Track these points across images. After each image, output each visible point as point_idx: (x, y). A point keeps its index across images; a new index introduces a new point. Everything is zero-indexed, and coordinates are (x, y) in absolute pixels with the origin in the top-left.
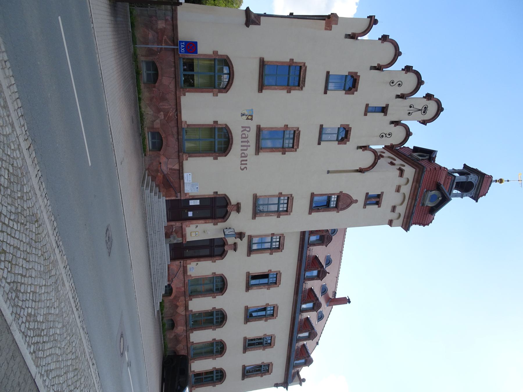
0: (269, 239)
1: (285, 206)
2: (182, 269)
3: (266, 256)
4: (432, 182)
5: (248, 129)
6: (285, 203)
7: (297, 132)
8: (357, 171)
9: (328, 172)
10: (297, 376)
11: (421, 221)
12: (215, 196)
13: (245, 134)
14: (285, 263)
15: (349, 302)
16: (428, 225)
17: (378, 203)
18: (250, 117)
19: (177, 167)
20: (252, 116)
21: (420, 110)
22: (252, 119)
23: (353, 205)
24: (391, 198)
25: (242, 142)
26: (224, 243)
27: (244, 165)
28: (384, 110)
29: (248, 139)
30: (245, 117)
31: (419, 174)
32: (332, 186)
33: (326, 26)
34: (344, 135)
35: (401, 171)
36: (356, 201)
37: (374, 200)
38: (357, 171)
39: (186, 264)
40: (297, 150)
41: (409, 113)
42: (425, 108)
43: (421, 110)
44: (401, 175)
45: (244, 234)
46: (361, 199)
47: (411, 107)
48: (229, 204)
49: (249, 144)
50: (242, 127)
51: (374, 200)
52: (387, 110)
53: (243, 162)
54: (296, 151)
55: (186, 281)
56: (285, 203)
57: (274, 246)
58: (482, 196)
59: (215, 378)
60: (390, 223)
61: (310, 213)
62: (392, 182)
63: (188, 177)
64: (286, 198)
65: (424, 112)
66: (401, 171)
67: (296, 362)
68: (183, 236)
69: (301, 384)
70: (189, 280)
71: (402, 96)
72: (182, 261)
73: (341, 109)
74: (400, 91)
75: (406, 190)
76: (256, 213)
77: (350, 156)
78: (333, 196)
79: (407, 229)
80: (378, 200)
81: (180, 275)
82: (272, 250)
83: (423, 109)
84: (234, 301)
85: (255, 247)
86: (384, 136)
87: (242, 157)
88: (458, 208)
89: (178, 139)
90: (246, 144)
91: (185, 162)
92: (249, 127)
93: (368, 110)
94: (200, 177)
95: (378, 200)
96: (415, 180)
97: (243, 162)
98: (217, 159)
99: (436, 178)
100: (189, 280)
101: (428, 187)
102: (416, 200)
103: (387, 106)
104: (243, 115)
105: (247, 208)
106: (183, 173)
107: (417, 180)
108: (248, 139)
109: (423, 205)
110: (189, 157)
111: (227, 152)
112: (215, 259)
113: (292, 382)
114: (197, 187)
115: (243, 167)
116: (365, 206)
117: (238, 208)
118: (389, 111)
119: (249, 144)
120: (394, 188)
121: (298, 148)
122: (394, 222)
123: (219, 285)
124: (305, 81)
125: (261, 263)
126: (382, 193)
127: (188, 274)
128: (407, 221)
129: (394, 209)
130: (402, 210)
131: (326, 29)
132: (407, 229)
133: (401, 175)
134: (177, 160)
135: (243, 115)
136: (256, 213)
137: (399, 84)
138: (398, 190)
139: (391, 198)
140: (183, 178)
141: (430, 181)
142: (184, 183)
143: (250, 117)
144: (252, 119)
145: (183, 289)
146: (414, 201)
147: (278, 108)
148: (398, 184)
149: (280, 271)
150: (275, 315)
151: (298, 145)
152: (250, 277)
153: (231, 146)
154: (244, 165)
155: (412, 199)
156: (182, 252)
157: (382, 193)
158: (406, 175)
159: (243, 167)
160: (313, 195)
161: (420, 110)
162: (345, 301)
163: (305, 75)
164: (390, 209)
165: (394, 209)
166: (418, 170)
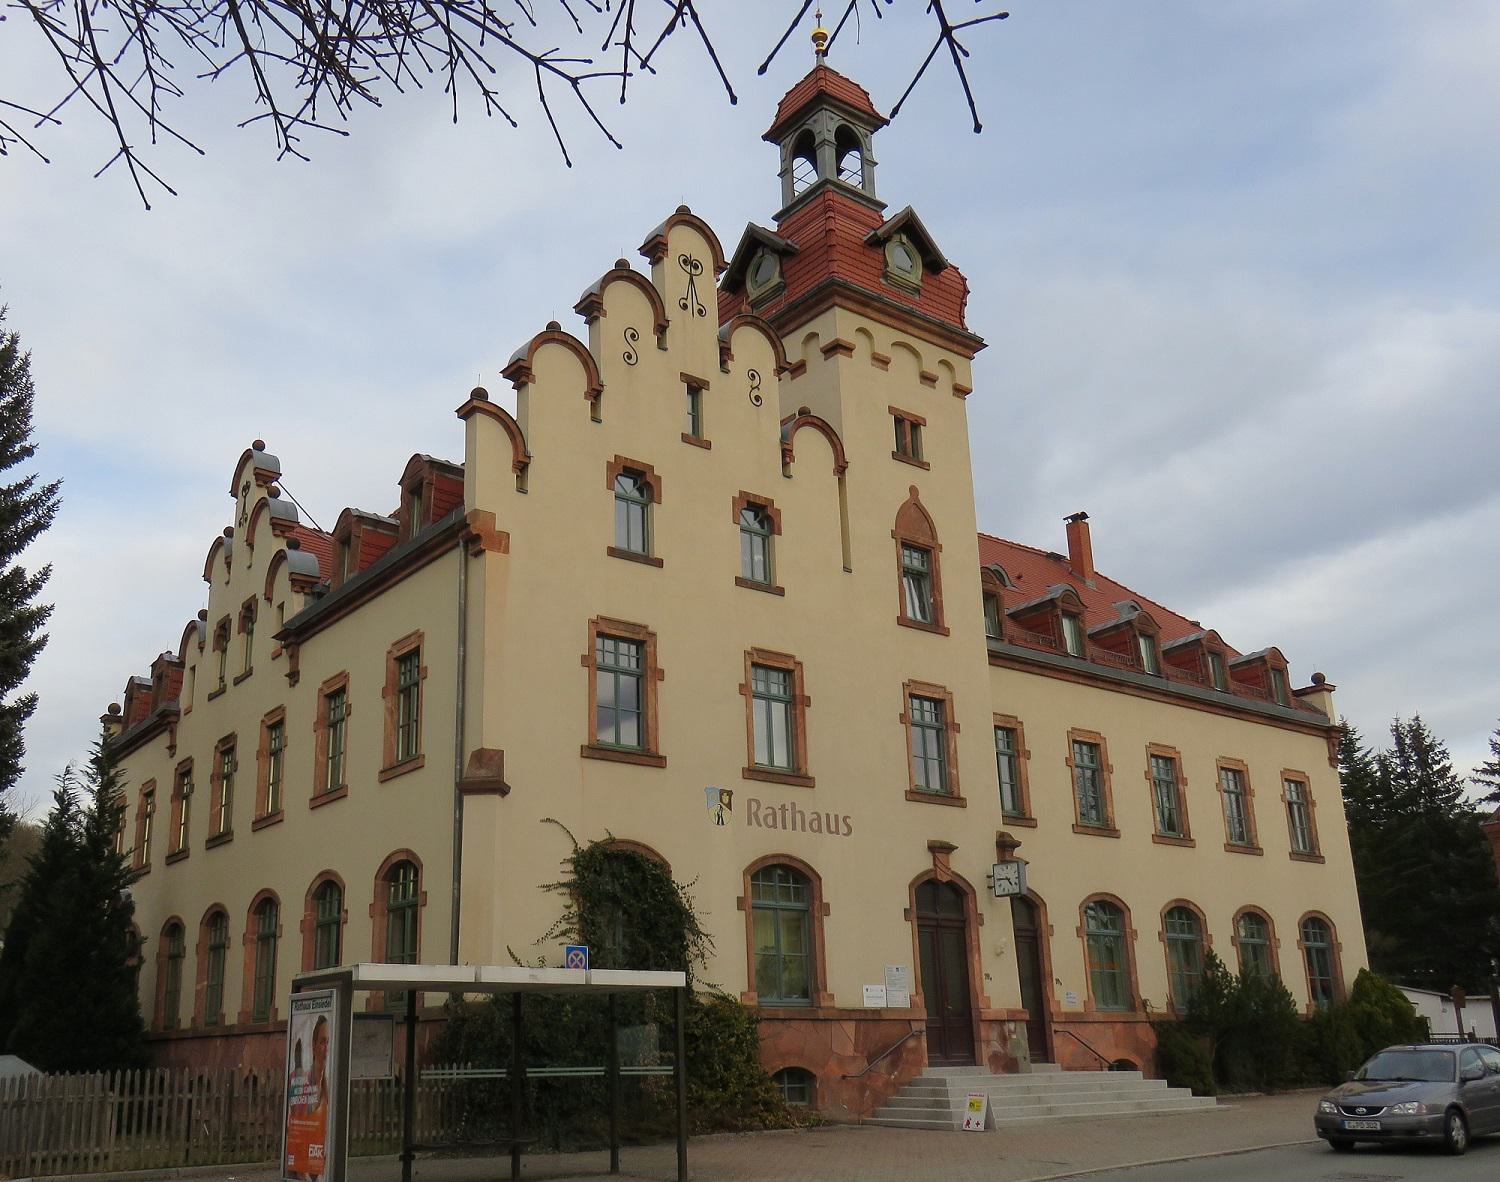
0: (606, 681)
1: (931, 711)
2: (1071, 1028)
3: (668, 699)
4: (863, 258)
5: (754, 804)
6: (616, 648)
7: (756, 659)
8: (841, 482)
9: (847, 569)
10: (1305, 699)
11: (954, 299)
12: (914, 916)
13: (766, 817)
14: (1055, 710)
15: (1084, 516)
16: (964, 280)
17: (916, 425)
18: (726, 799)
19: (850, 1028)
20: (722, 792)
21: (691, 280)
22: (730, 793)
23: (924, 500)
24: (901, 387)
25: (784, 827)
26: (929, 882)
27: (835, 825)
28: (695, 387)
29: (777, 807)
30: (726, 813)
31: (848, 298)
32: (881, 560)
33: (499, 550)
34: (761, 515)
35: (835, 348)
36: (913, 490)
37: (908, 431)
38: (841, 482)
39: (1060, 1014)
40: (798, 659)
41: (700, 312)
42: (685, 262)
43: (691, 276)
44: (848, 349)
45: (1001, 835)
46: (907, 474)
47: (685, 307)
48: (932, 875)
49: (788, 806)
50: (750, 823)
51: (908, 431)
52: (696, 380)
53: (833, 829)
54: (800, 664)
55: (1099, 1016)
56: (616, 648)
57: (1232, 784)
58: (871, 104)
59: (1320, 944)
60: (961, 391)
61: (945, 633)
62: (867, 374)
63: (874, 997)
64: (599, 641)
65: (696, 267)
66: (835, 348)
67: (1146, 668)
68: (1013, 1017)
69: (1331, 689)
70: (1098, 1010)
71: (661, 328)
72: (1054, 1027)
73: (696, 522)
74: (648, 337)
75: (885, 337)
76: (949, 796)
77: (807, 497)
78: (907, 561)
79: (977, 344)
80: (907, 423)
81: (1086, 1033)
82: (646, 674)
83: (688, 268)
84: (1144, 874)
85: (629, 737)
86: (755, 393)
87: (820, 830)
88: (899, 173)
89: (784, 1020)
90: (788, 815)
91: (839, 1003)
92: (750, 801)
93: (695, 438)
94: (871, 964)
95: (907, 423)
96: (861, 309)
97: (833, 829)
98: (828, 905)
99: (853, 246)
100: (1098, 1010)
101: (876, 272)
102: (910, 313)
103: (685, 377)
104: (720, 820)
105: (940, 822)
106: (865, 1011)
107: (864, 303)
108: (777, 807)
109: (917, 290)
110: (826, 990)
111: (809, 873)
112: (1044, 927)
113: (1326, 715)
114: (895, 970)
115: (843, 829)
116: (924, 466)
117: (940, 849)
118: (696, 372)
119: (788, 806)
120: (877, 371)
121: (792, 657)
122: (961, 381)
123: (1107, 913)
124: (634, 625)
125: (1052, 786)
126: (891, 410)
127: (1081, 1009)
128: (959, 344)
129: (928, 379)
130: (932, 355)
131: (506, 550)
132: (977, 344)
133: (848, 349)
134: (835, 1026)
135: (720, 820)
136: (949, 796)
137: (633, 336)
138: (883, 362)
139: (901, 387)
140: (877, 1011)
141: (850, 261)
142: (888, 1009)
143: (726, 799)
144: (730, 793)
145: (1119, 1027)
146: (914, 319)
147: (704, 712)
148: (868, 360)
149: (593, 622)
150: (791, 666)
151: (786, 656)
152: (1171, 833)
153: (796, 859)
154: (835, 825)
155: (906, 322)
156: (1040, 1029)
157: (891, 410)
158: (847, 335)
159: (843, 829)
160: (903, 621)
161: (691, 280)
162: (1077, 524)
163: (620, 622)
164: (926, 389)
165: (928, 379)
166: (838, 300)
